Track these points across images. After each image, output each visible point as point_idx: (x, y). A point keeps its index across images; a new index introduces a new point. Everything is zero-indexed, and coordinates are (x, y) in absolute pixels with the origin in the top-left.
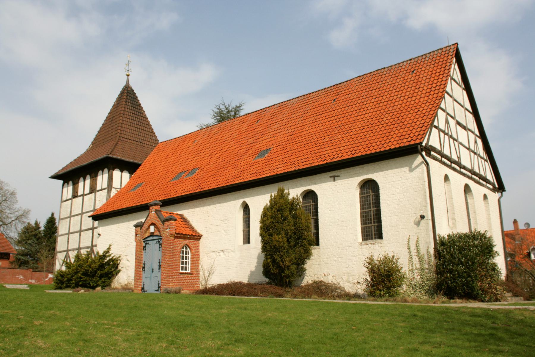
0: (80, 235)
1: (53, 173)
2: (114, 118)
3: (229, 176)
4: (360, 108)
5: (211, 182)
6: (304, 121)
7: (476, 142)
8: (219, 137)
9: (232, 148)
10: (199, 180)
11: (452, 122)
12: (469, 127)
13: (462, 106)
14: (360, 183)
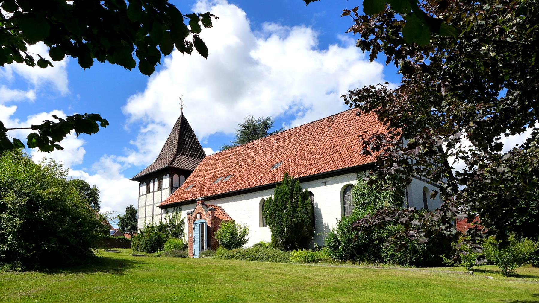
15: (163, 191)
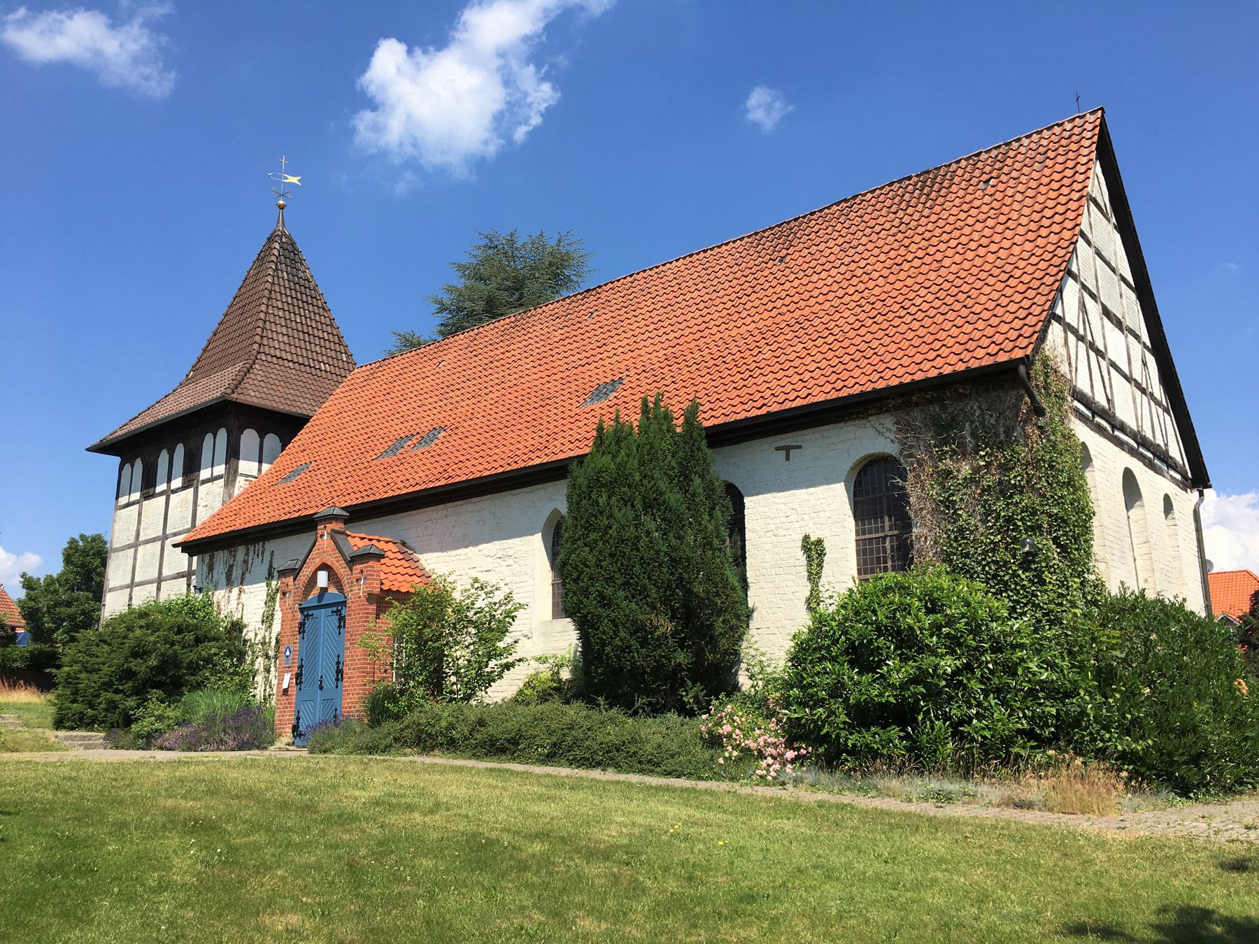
0: (159, 589)
1: (95, 441)
2: (247, 308)
3: (519, 446)
4: (848, 275)
5: (475, 462)
6: (706, 311)
7: (1145, 364)
8: (497, 352)
9: (527, 378)
10: (445, 457)
11: (1093, 309)
12: (1128, 322)
13: (1113, 270)
14: (852, 468)
15: (202, 489)
